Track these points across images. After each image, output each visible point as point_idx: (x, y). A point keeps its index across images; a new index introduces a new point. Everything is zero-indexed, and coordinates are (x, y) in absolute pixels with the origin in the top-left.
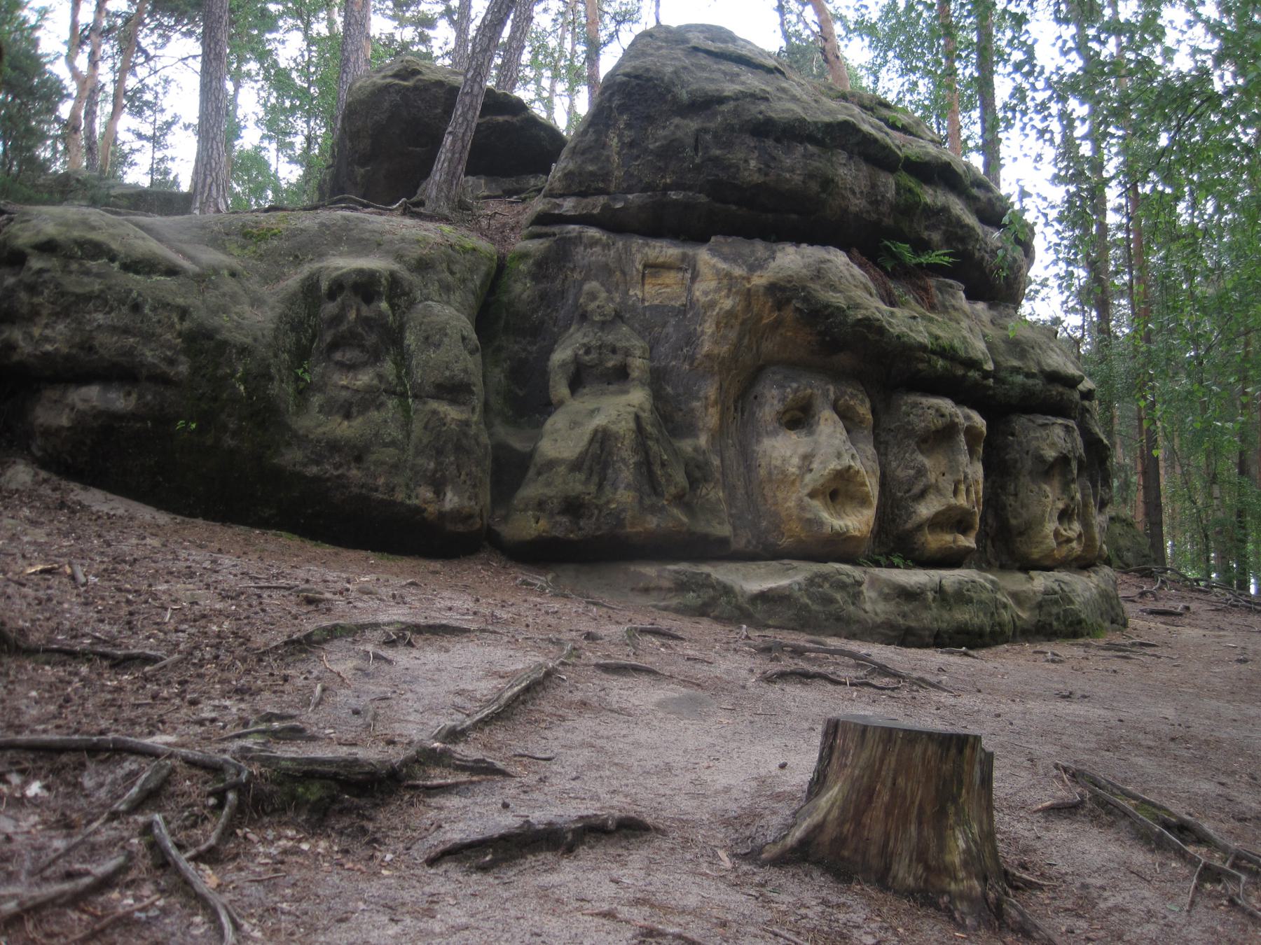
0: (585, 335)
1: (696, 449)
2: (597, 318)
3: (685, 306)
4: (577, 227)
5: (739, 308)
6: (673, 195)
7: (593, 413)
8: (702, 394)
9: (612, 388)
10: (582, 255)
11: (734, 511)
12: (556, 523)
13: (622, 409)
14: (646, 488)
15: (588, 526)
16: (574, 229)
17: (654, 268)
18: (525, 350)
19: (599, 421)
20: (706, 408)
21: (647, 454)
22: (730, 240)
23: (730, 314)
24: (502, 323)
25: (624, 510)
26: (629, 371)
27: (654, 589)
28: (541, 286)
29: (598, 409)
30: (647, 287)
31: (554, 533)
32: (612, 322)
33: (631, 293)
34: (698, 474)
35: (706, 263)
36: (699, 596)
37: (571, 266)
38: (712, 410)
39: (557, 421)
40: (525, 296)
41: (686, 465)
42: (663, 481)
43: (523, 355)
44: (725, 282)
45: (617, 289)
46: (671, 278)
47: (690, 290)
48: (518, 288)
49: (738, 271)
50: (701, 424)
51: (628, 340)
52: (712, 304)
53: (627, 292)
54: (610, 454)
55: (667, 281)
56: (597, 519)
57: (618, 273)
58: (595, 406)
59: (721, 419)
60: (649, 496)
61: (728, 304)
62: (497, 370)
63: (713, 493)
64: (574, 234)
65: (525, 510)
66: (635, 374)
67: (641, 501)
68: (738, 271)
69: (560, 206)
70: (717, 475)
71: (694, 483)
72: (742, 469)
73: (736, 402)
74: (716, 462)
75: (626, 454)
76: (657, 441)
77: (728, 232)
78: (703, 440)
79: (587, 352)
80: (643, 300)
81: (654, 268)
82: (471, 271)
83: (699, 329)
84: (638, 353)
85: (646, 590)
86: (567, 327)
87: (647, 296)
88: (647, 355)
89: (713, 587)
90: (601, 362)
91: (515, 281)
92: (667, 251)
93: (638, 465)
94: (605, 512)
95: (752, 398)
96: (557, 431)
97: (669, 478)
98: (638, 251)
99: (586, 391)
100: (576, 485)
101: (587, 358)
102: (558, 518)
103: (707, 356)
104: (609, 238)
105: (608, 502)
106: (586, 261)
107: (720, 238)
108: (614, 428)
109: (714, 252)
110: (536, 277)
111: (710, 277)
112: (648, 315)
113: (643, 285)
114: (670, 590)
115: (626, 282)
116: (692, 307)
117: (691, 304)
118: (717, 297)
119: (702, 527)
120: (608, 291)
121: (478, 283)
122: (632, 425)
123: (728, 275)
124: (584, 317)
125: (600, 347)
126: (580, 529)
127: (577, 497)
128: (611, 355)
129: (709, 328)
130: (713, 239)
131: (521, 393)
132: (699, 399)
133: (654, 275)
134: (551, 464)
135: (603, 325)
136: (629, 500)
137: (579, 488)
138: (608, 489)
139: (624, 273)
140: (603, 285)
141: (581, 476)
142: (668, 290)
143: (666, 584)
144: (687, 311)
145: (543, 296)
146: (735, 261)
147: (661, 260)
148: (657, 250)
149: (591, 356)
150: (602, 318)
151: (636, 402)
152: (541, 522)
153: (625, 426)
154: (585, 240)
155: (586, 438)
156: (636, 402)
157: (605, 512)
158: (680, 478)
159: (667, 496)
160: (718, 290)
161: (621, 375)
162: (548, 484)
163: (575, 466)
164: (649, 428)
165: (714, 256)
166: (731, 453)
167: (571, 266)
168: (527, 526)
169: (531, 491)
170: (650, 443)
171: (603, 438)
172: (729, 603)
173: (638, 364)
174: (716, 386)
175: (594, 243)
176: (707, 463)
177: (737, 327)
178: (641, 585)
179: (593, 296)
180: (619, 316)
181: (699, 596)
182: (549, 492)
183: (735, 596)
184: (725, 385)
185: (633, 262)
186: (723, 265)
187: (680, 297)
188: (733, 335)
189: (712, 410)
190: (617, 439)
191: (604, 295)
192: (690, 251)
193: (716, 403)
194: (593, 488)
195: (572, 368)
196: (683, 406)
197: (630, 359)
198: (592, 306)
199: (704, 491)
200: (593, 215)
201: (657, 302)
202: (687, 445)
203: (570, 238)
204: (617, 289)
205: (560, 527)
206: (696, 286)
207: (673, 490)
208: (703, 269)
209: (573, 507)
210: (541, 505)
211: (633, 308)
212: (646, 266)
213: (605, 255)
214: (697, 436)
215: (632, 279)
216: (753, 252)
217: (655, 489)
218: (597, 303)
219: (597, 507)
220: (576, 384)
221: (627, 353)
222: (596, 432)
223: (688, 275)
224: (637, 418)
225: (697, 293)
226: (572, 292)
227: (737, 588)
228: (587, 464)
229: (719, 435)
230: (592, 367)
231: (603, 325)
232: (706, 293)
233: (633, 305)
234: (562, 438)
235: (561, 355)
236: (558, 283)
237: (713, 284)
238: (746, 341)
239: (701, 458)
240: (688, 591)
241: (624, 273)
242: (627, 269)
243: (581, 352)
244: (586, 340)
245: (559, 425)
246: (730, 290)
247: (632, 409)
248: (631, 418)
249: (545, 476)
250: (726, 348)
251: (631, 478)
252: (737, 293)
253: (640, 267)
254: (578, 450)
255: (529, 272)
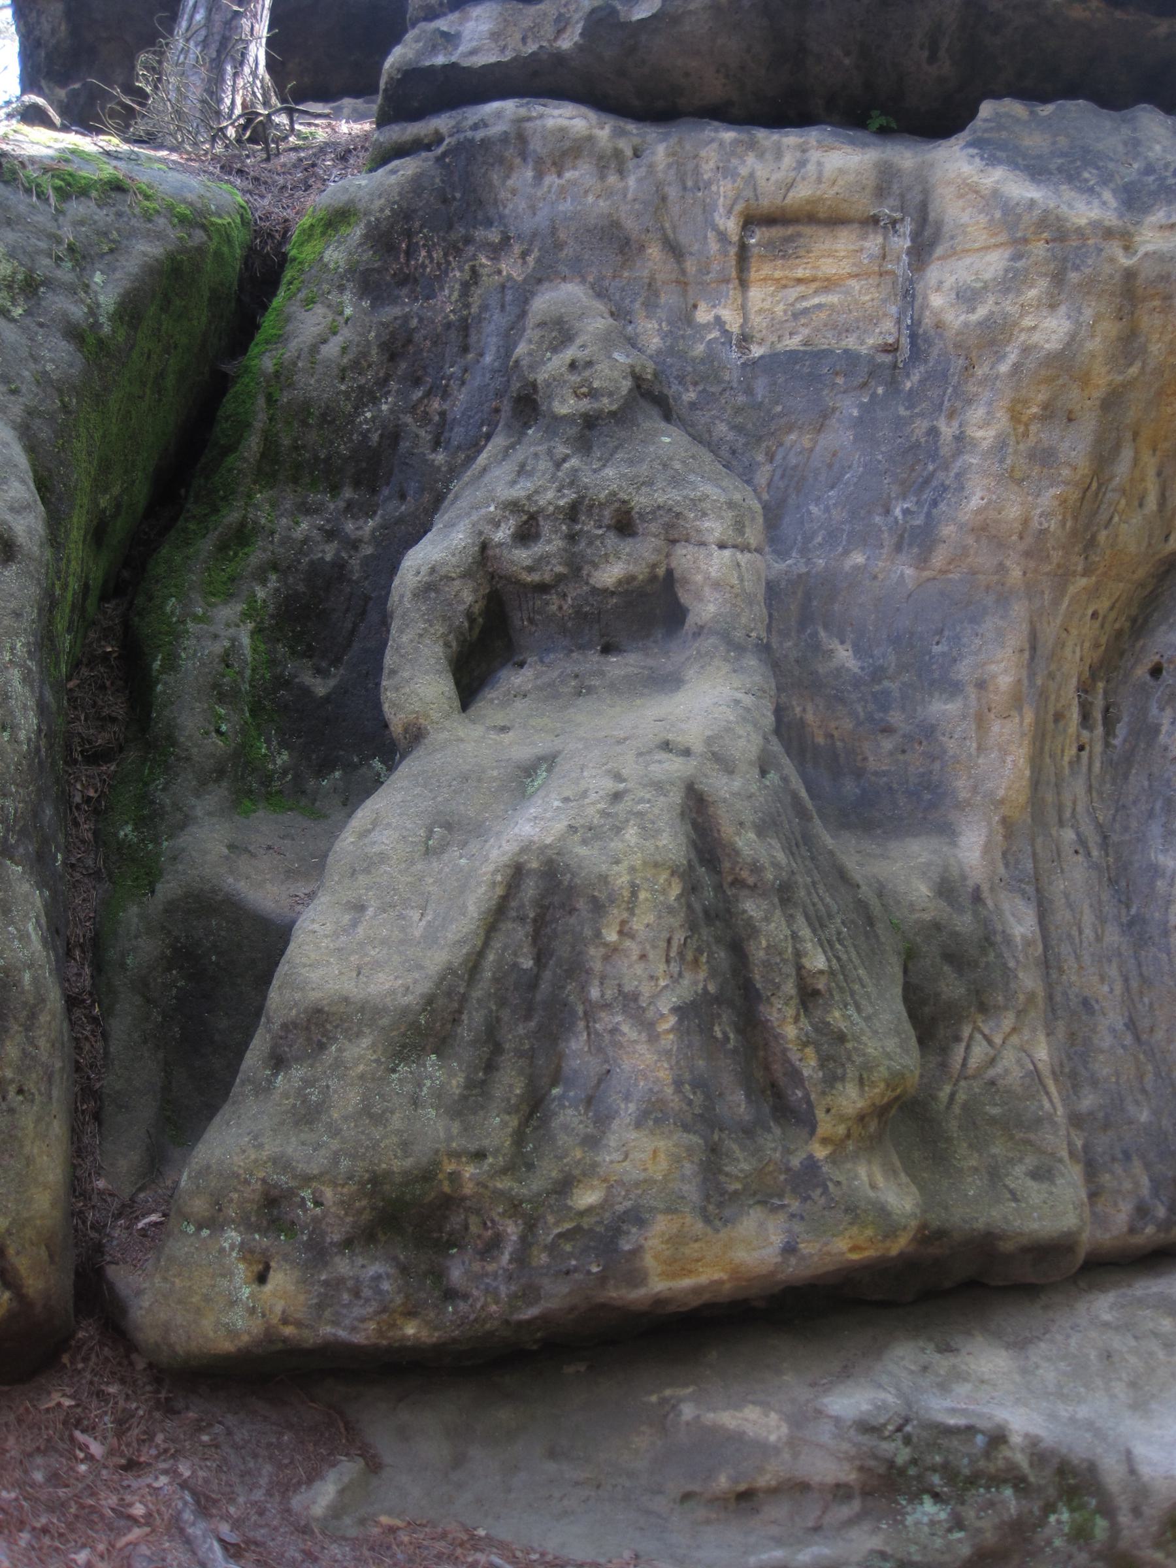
0: (522, 471)
1: (946, 889)
2: (566, 406)
3: (891, 349)
4: (509, 107)
5: (1094, 345)
6: (948, 1089)
7: (525, 777)
8: (963, 670)
9: (618, 666)
10: (526, 197)
11: (1088, 1101)
12: (336, 1284)
13: (630, 767)
14: (737, 1103)
15: (484, 1291)
16: (501, 112)
17: (778, 224)
18: (331, 535)
19: (534, 825)
20: (981, 721)
21: (738, 950)
22: (1047, 110)
23: (1063, 364)
24: (253, 444)
25: (637, 1217)
26: (684, 598)
27: (774, 1491)
28: (391, 312)
29: (549, 760)
30: (756, 294)
31: (327, 1330)
32: (622, 417)
33: (703, 315)
34: (952, 987)
35: (968, 189)
36: (958, 1523)
37: (494, 236)
38: (1000, 730)
39: (386, 819)
40: (331, 350)
41: (910, 956)
42: (809, 1066)
43: (329, 552)
44: (1039, 249)
45: (650, 306)
46: (837, 254)
47: (909, 295)
48: (309, 324)
49: (1085, 211)
50: (961, 785)
51: (676, 481)
52: (994, 335)
53: (687, 317)
54: (576, 970)
55: (829, 268)
56: (521, 1258)
57: (654, 252)
58: (542, 745)
59: (1036, 761)
60: (748, 1132)
61: (1051, 330)
62: (229, 612)
63: (1011, 1050)
64: (496, 130)
65: (214, 1223)
66: (706, 608)
67: (712, 1163)
68: (1085, 211)
69: (449, 39)
70: (1029, 981)
71: (931, 1022)
72: (1113, 937)
73: (1084, 689)
74: (1020, 923)
75: (644, 971)
76: (785, 894)
77: (1042, 83)
78: (972, 848)
79: (526, 535)
80: (745, 339)
81: (778, 224)
82: (80, 256)
83: (948, 431)
84: (715, 527)
85: (745, 1499)
86: (475, 447)
87: (758, 322)
88: (753, 535)
89: (1020, 1483)
90: (576, 568)
91: (310, 302)
92: (833, 162)
93: (693, 1014)
94: (553, 1227)
95: (1141, 672)
96: (370, 864)
97: (833, 1047)
98: (725, 170)
99: (517, 679)
100: (422, 1121)
101: (523, 555)
102: (343, 1266)
103: (981, 529)
104: (619, 133)
105: (565, 1186)
106: (541, 219)
107: (1015, 108)
108: (587, 857)
109: (992, 150)
110: (370, 285)
111: (982, 238)
112: (761, 388)
113: (744, 284)
114: (840, 1492)
115: (682, 284)
116: (917, 354)
117: (919, 338)
118: (1010, 306)
119: (975, 1208)
120: (620, 314)
121: (108, 300)
122: (671, 842)
123: (1055, 230)
124: (527, 406)
125: (573, 512)
126: (450, 1295)
127: (428, 1175)
128: (612, 539)
129: (984, 424)
130: (987, 109)
131: (321, 688)
132: (954, 689)
133: (781, 251)
134: (319, 1027)
135: (590, 430)
136: (659, 1169)
137: (435, 1129)
138: (569, 1119)
139: (675, 251)
140: (600, 293)
141: (441, 1075)
142: (833, 299)
143: (826, 1468)
144: (911, 369)
145: (396, 346)
146: (1071, 177)
147: (802, 192)
148: (788, 160)
149: (538, 549)
150: (585, 405)
151: (693, 734)
152: (280, 1279)
153: (638, 856)
154: (536, 145)
155: (476, 903)
156: (693, 734)
157: (553, 1227)
158: (880, 1034)
159: (826, 1126)
160: (1011, 282)
161: (652, 613)
162: (307, 1115)
163: (422, 1032)
164: (746, 843)
165: (992, 162)
166: (1074, 880)
167: (494, 236)
168: (215, 1291)
169: (240, 1142)
170: (752, 907)
171: (545, 907)
172: (1080, 1534)
173: (717, 571)
174: (1016, 638)
175: (569, 151)
176: (989, 938)
177: (1088, 426)
178: (723, 1482)
179: (561, 332)
180: (650, 395)
181: (958, 1523)
182: (306, 1152)
183: (1107, 1510)
184: (1050, 631)
185: (708, 209)
186: (1022, 190)
187: (873, 320)
188: (1075, 448)
189: (1000, 730)
190: (598, 908)
191: (598, 323)
192: (905, 156)
193: (1017, 701)
194: (497, 1128)
195: (467, 596)
196: (895, 717)
197: (684, 557)
198: (557, 363)
199: (979, 1051)
200: (559, 59)
201: (793, 343)
202: (906, 871)
203: (485, 143)
204: (650, 306)
205: (369, 1300)
206: (933, 273)
207: (851, 1099)
208: (954, 211)
209: (411, 1217)
210: (273, 1209)
211: (708, 372)
212: (750, 221)
213: (609, 193)
214: (948, 831)
215: (704, 269)
216: (1134, 145)
217: (781, 1103)
218: (570, 353)
219: (514, 1207)
220: (482, 654)
221: (675, 532)
222: (517, 873)
223: (902, 243)
224: (697, 807)
225: (937, 301)
226: (496, 321)
227: (1112, 1472)
228: (473, 1021)
229: (1027, 832)
230: (542, 588)
231: (590, 430)
232: (967, 297)
233: (710, 357)
234: (370, 913)
235: (438, 550)
236: (446, 303)
237: (994, 263)
238: (1122, 468)
239: (964, 923)
240: (915, 1497)
241: (675, 251)
242: (684, 238)
243: (502, 534)
244: (519, 491)
245: (384, 840)
246: (1058, 279)
247: (673, 767)
248: (664, 809)
249: (298, 1072)
250: (1049, 497)
251: (664, 1074)
252: (1088, 287)
253: (731, 226)
254: (437, 959)
255: (352, 270)
